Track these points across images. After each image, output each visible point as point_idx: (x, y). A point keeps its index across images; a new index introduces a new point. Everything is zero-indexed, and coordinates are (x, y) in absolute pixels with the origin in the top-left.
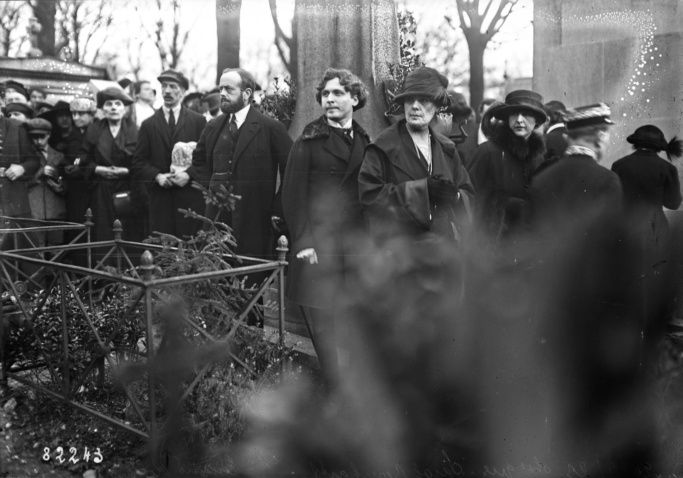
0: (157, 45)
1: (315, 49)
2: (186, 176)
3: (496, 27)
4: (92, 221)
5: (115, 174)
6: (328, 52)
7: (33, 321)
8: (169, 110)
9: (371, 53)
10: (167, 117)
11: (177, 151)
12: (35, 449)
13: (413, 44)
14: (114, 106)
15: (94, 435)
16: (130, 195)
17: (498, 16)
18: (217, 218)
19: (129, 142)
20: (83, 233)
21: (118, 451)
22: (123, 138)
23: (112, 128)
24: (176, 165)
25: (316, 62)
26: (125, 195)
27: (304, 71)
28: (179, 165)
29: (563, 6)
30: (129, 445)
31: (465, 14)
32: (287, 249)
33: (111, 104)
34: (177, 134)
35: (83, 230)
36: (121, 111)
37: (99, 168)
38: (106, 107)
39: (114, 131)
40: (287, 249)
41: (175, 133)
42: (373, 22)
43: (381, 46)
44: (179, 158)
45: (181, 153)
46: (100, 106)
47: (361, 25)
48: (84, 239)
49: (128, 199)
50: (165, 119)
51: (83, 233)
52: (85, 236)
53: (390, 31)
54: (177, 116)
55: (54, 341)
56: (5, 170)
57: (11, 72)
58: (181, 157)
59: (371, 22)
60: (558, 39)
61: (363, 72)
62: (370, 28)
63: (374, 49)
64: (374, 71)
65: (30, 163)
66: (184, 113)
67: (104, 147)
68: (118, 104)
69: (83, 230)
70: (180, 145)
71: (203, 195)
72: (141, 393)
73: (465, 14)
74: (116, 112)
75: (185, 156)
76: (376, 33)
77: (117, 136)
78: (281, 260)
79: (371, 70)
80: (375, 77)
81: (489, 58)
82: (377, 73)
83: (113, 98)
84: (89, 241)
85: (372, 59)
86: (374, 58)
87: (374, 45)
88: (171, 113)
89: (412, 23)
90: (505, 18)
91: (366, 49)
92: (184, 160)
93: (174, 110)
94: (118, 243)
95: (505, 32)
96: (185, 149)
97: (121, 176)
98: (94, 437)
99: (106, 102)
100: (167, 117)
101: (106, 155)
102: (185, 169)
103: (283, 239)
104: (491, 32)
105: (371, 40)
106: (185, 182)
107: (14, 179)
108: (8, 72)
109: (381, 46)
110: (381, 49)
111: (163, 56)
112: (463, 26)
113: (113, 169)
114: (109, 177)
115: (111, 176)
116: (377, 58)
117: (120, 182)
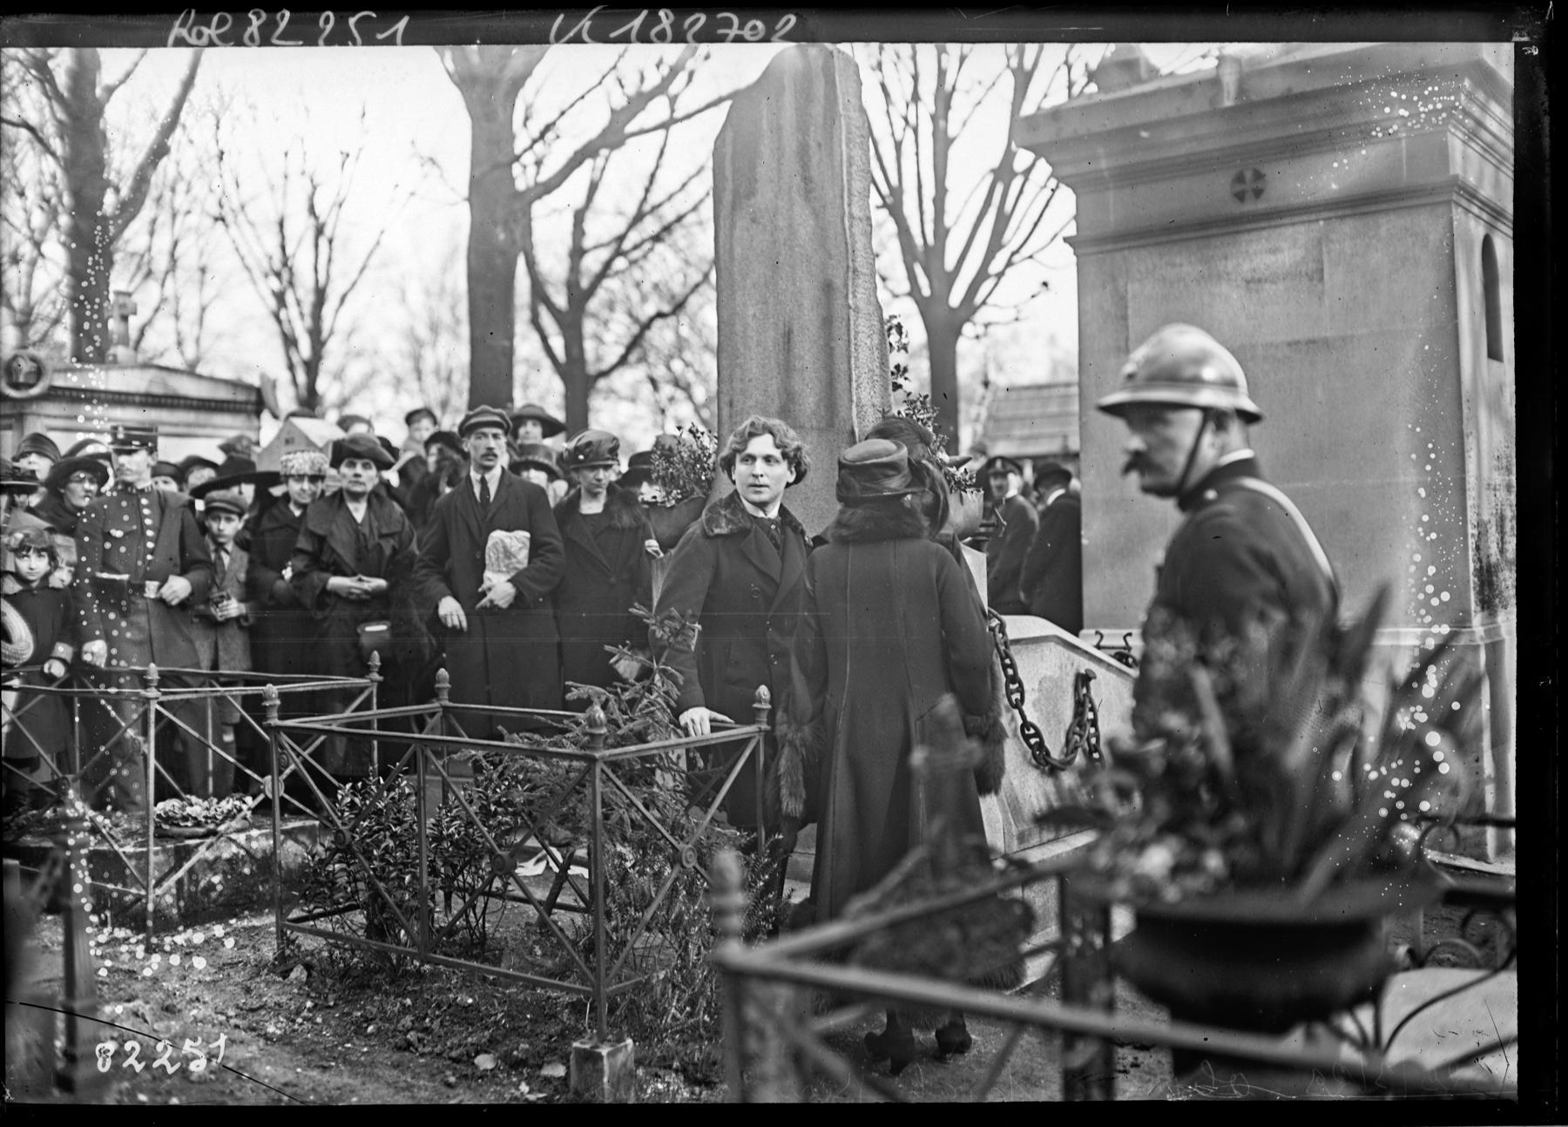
0: (277, 316)
1: (750, 381)
2: (510, 590)
3: (978, 299)
4: (380, 673)
5: (366, 592)
6: (774, 386)
7: (353, 830)
8: (479, 477)
9: (850, 391)
10: (477, 490)
11: (495, 545)
12: (372, 1034)
13: (905, 370)
14: (359, 469)
15: (467, 1008)
16: (391, 628)
17: (982, 275)
18: (663, 660)
19: (385, 531)
20: (366, 694)
21: (514, 1029)
22: (375, 524)
23: (351, 506)
24: (494, 571)
25: (751, 403)
26: (382, 627)
27: (731, 417)
28: (499, 571)
29: (1129, 287)
30: (530, 1020)
31: (918, 269)
32: (769, 706)
33: (352, 465)
34: (492, 518)
35: (366, 688)
36: (371, 479)
37: (336, 581)
38: (344, 469)
39: (356, 510)
40: (769, 706)
41: (490, 515)
42: (853, 341)
43: (864, 378)
44: (498, 559)
45: (501, 550)
46: (335, 463)
47: (833, 344)
48: (365, 705)
49: (387, 636)
50: (473, 493)
51: (366, 694)
52: (368, 700)
53: (876, 353)
54: (493, 488)
55: (389, 863)
56: (160, 587)
57: (110, 397)
58: (501, 556)
59: (849, 341)
60: (1122, 344)
61: (837, 421)
62: (848, 350)
63: (854, 385)
64: (855, 420)
65: (199, 575)
66: (506, 482)
67: (342, 545)
68: (365, 466)
69: (366, 688)
70: (497, 535)
71: (647, 626)
72: (530, 943)
73: (918, 269)
74: (361, 480)
75: (508, 554)
76: (857, 359)
77: (364, 520)
78: (759, 722)
79: (851, 419)
80: (857, 430)
81: (969, 356)
82: (860, 423)
83: (359, 456)
84: (375, 706)
85: (851, 401)
86: (854, 398)
87: (854, 377)
88: (483, 482)
89: (900, 333)
90: (1000, 275)
91: (841, 386)
92: (507, 561)
93: (487, 476)
94: (445, 708)
95: (1000, 302)
96: (507, 541)
97: (376, 595)
98: (467, 1012)
99: (346, 461)
100: (477, 490)
101: (347, 556)
102: (509, 577)
103: (763, 691)
104: (969, 307)
105: (850, 369)
106: (510, 599)
107: (174, 602)
108: (150, 400)
109: (864, 378)
110: (865, 384)
111: (290, 341)
112: (914, 292)
113: (360, 580)
114: (353, 597)
115: (358, 595)
116: (859, 398)
117: (371, 605)
